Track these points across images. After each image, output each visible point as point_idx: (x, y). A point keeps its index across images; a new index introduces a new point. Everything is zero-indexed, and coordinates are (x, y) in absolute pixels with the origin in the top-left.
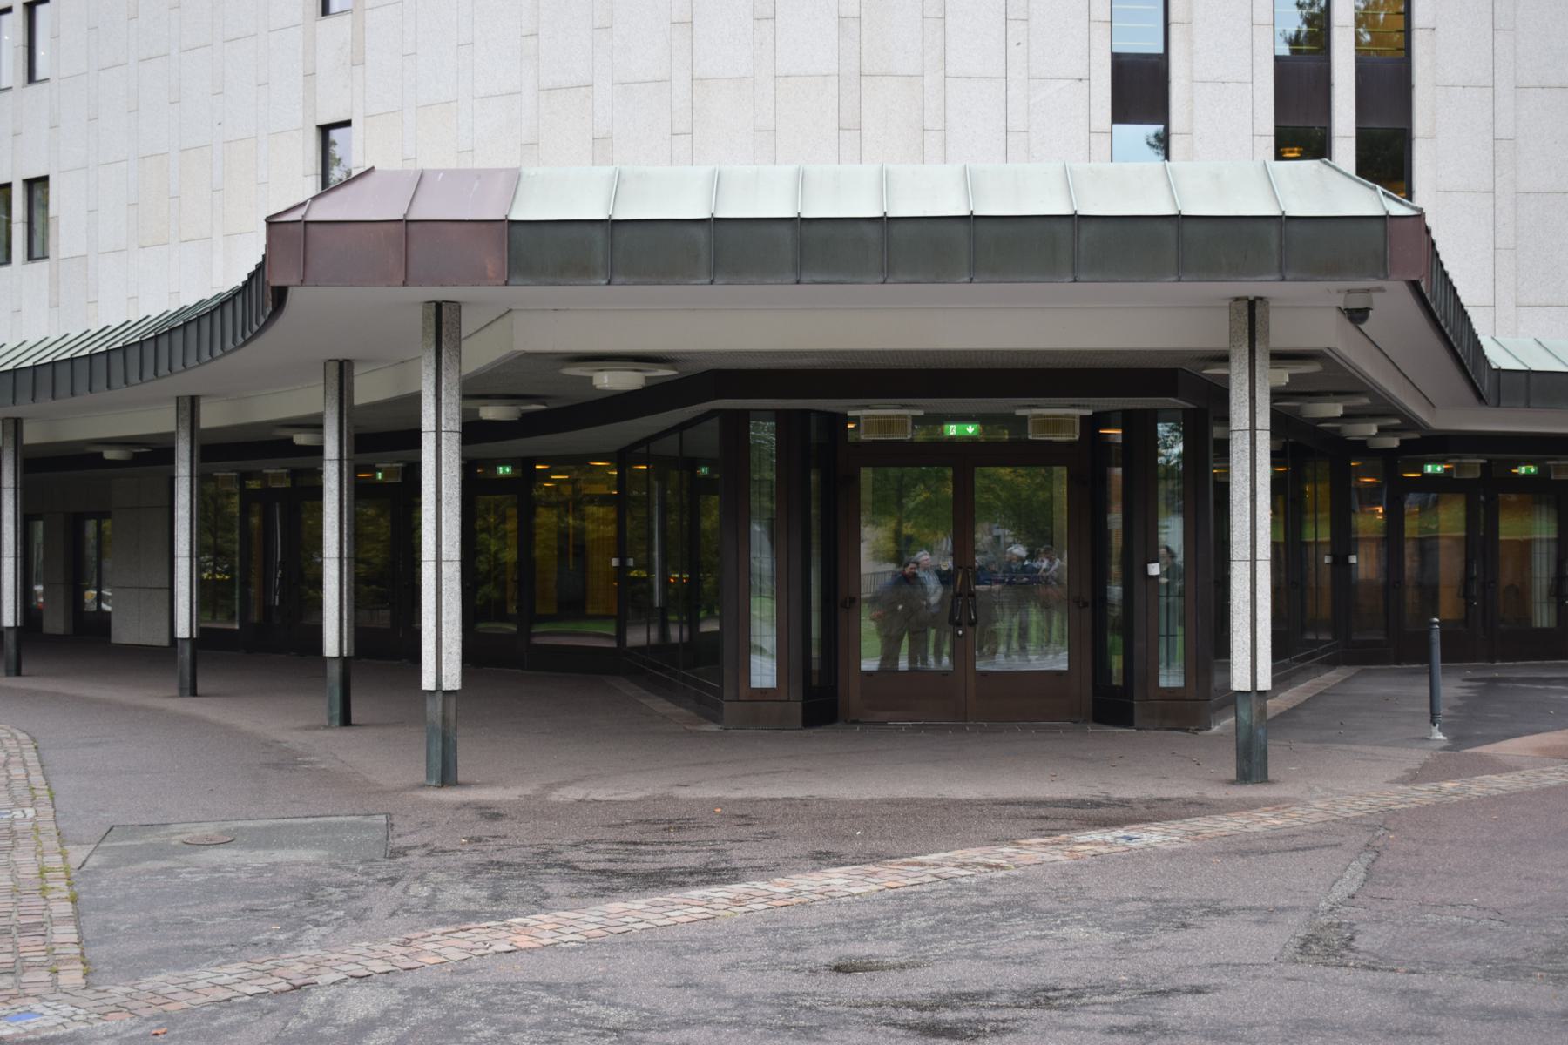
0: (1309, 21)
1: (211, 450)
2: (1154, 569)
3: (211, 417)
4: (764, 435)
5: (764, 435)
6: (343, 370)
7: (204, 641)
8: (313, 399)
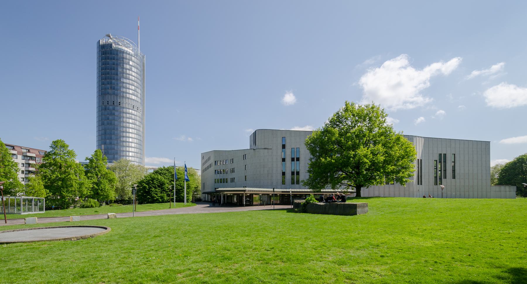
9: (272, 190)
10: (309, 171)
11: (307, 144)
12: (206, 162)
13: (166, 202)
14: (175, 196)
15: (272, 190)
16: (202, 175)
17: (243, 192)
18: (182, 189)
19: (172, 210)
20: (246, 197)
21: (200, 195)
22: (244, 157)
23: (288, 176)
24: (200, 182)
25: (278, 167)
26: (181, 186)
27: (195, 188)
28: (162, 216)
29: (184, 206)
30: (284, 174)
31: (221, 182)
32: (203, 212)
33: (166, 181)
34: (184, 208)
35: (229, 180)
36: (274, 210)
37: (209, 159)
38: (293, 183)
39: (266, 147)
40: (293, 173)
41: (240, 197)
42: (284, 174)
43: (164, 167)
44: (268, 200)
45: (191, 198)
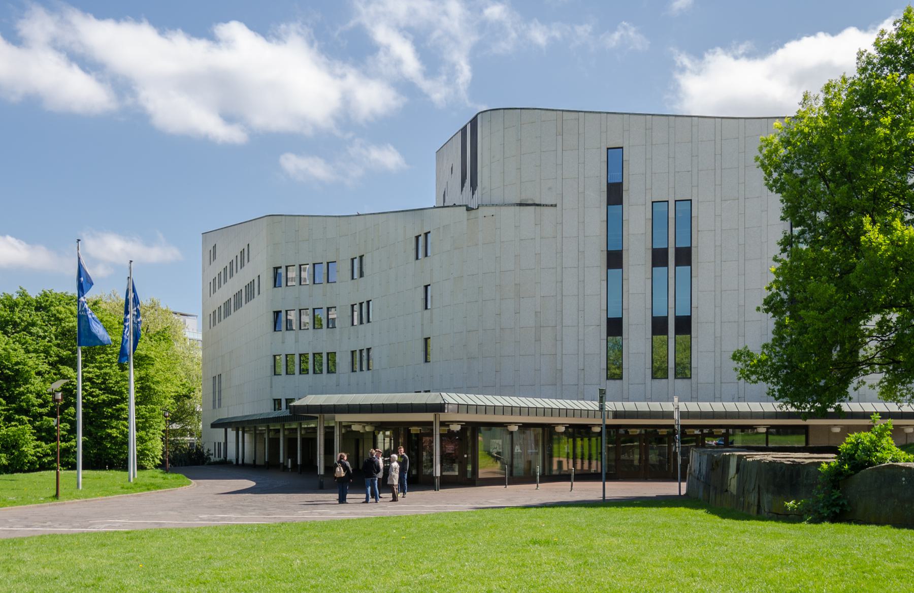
2: (846, 467)
9: (594, 405)
10: (772, 306)
11: (769, 163)
12: (229, 272)
13: (32, 468)
14: (80, 438)
15: (594, 405)
16: (204, 341)
17: (428, 417)
18: (110, 403)
19: (66, 506)
20: (448, 436)
21: (199, 434)
22: (421, 244)
23: (637, 341)
24: (197, 370)
25: (585, 296)
26: (108, 390)
27: (178, 398)
28: (17, 542)
29: (126, 488)
30: (615, 327)
31: (304, 371)
32: (234, 518)
33: (34, 363)
34: (131, 499)
35: (343, 362)
36: (605, 503)
37: (244, 257)
38: (659, 372)
39: (527, 196)
40: (659, 326)
41: (413, 440)
42: (615, 327)
43: (23, 295)
44: (547, 452)
45: (157, 446)
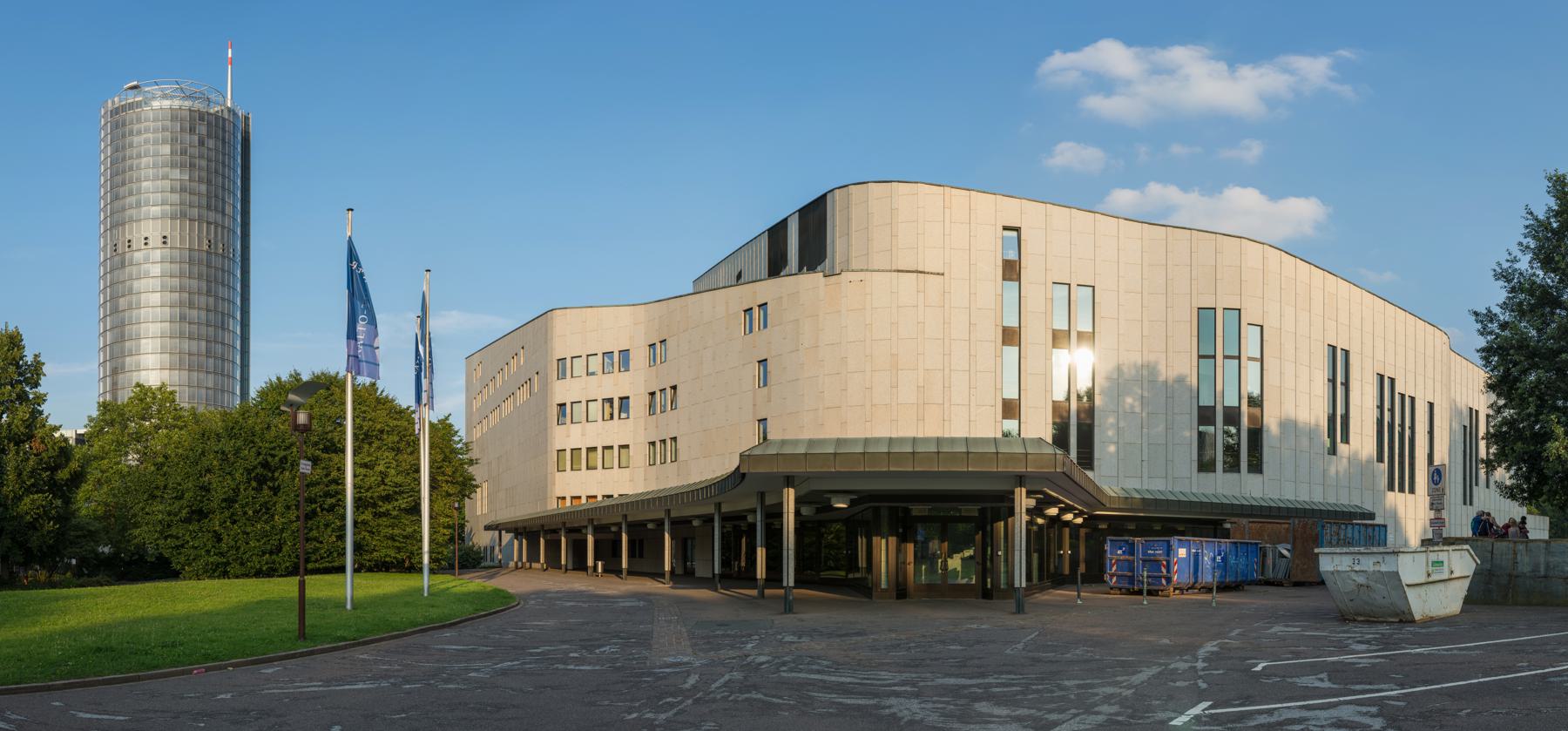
0: (118, 520)
1: (725, 518)
3: (724, 509)
4: (884, 513)
5: (884, 513)
6: (762, 495)
7: (723, 576)
8: (752, 502)
